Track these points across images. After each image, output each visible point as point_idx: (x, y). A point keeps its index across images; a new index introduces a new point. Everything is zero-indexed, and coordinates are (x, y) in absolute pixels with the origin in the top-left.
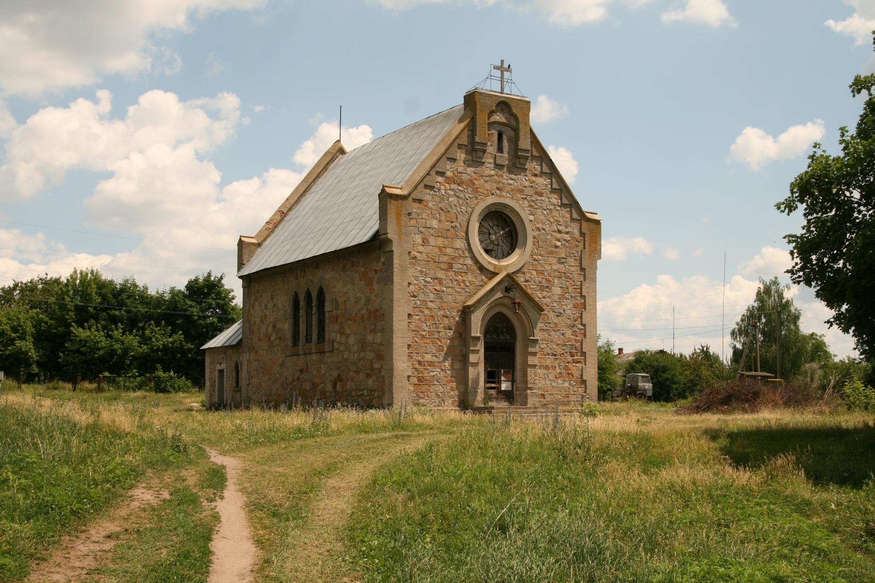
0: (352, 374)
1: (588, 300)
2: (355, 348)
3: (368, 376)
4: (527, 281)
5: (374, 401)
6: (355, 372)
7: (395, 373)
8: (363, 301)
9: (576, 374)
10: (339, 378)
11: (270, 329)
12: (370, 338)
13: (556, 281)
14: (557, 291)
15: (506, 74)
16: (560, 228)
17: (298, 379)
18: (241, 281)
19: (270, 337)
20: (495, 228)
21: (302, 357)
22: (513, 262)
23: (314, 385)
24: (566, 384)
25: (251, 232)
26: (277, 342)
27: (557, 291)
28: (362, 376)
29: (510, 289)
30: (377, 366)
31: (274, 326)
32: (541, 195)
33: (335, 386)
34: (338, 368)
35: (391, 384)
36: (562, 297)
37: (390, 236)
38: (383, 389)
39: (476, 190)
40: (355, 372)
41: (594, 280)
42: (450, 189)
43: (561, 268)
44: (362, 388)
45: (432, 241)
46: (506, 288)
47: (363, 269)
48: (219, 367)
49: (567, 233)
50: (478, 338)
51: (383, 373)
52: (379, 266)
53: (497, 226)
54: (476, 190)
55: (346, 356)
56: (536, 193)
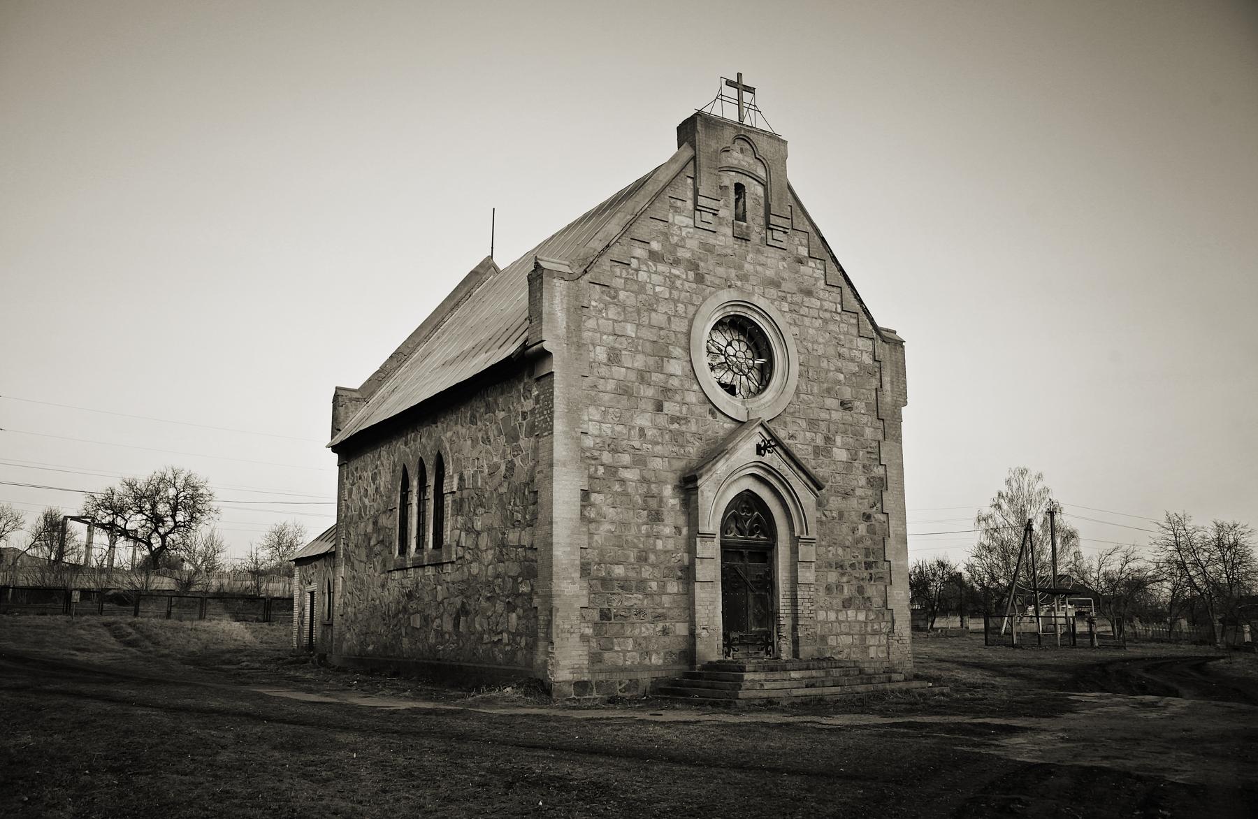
0: (484, 604)
1: (892, 473)
2: (489, 556)
3: (511, 607)
4: (792, 437)
5: (519, 654)
6: (488, 599)
7: (556, 602)
8: (503, 467)
9: (877, 602)
10: (463, 611)
11: (370, 528)
12: (512, 537)
13: (838, 439)
14: (841, 455)
15: (747, 96)
16: (842, 350)
17: (405, 609)
18: (336, 456)
19: (370, 540)
20: (735, 344)
21: (411, 572)
22: (767, 405)
23: (426, 620)
24: (862, 617)
25: (355, 382)
26: (378, 548)
27: (841, 455)
28: (500, 607)
29: (765, 448)
30: (524, 589)
31: (375, 523)
32: (809, 293)
33: (456, 625)
34: (462, 592)
35: (549, 623)
36: (849, 465)
37: (547, 346)
38: (534, 635)
39: (700, 279)
40: (488, 599)
41: (898, 439)
42: (655, 272)
43: (847, 416)
44: (500, 628)
45: (626, 360)
46: (758, 446)
47: (501, 415)
48: (310, 588)
49: (852, 360)
50: (712, 536)
51: (536, 601)
52: (528, 405)
53: (739, 341)
54: (700, 279)
55: (475, 570)
56: (801, 291)
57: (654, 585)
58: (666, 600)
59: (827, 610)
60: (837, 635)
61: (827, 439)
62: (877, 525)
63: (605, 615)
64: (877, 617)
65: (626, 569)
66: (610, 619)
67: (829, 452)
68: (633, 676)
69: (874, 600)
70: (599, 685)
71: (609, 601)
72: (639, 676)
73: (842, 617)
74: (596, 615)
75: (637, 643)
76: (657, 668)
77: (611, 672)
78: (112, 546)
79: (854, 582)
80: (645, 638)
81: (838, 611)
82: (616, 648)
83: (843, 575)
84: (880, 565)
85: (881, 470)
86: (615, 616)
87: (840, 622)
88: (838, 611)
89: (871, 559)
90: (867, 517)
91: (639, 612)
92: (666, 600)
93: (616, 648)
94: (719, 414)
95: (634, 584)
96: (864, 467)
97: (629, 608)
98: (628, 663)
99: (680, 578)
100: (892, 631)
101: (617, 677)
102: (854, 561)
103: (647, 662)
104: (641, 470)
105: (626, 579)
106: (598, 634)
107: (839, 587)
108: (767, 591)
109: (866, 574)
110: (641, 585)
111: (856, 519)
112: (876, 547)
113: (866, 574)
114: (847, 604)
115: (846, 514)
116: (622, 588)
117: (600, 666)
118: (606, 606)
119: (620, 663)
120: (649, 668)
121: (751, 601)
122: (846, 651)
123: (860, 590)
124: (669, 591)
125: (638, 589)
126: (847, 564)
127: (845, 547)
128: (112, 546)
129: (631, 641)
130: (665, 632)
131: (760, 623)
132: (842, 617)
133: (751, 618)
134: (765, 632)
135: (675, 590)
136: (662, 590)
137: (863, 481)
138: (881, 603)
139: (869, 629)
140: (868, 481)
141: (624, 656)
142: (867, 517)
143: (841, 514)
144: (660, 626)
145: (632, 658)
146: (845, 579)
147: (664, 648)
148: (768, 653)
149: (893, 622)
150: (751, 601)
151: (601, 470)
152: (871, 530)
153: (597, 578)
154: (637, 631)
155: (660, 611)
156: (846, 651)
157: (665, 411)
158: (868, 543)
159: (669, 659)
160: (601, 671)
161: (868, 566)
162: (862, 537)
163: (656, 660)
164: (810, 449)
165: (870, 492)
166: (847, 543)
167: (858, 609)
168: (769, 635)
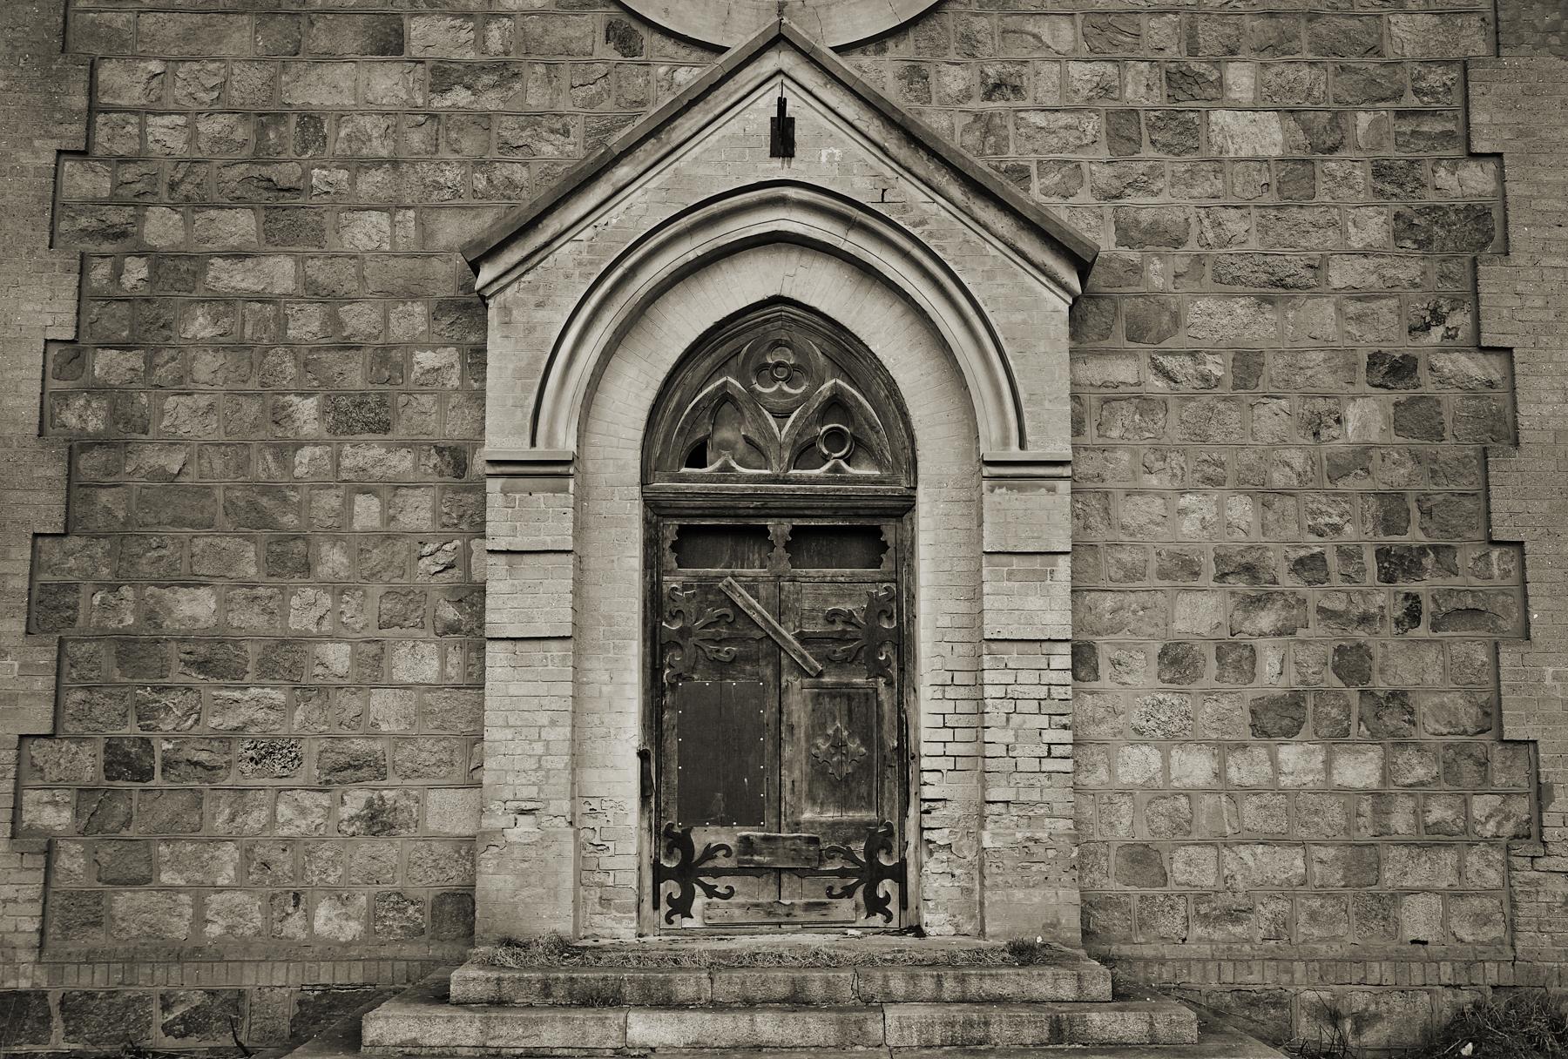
13: (1241, 79)
14: (1250, 132)
36: (1295, 175)
57: (337, 657)
58: (386, 708)
59: (1171, 740)
60: (1220, 843)
61: (1179, 80)
62: (1452, 400)
63: (126, 763)
64: (1449, 771)
65: (225, 603)
66: (147, 775)
67: (1188, 129)
68: (222, 979)
69: (1424, 705)
70: (74, 1007)
71: (145, 713)
72: (249, 979)
73: (1241, 771)
74: (88, 764)
75: (254, 864)
76: (334, 952)
77: (131, 960)
78: (1166, 759)
79: (1316, 629)
80: (289, 842)
81: (1224, 749)
82: (166, 878)
83: (1257, 602)
84: (1466, 557)
85: (1477, 180)
86: (168, 765)
87: (1236, 793)
88: (1224, 749)
89: (1415, 536)
90: (1394, 370)
91: (265, 753)
92: (386, 708)
93: (166, 878)
94: (651, 40)
95: (252, 651)
96: (1380, 171)
97: (226, 739)
98: (214, 930)
99: (452, 628)
100: (1531, 834)
101: (151, 980)
102: (1314, 544)
103: (294, 927)
104: (300, 261)
105: (220, 638)
106: (91, 825)
107: (1236, 655)
108: (879, 670)
109: (1384, 599)
110: (285, 658)
111: (1327, 381)
112: (1437, 490)
113: (1384, 599)
114: (1278, 719)
115: (1275, 366)
116: (203, 666)
117: (97, 939)
118: (132, 729)
119: (180, 928)
120: (291, 953)
121: (798, 707)
122: (1267, 910)
123: (1352, 664)
124: (401, 674)
125: (267, 670)
126: (1277, 560)
127: (1265, 495)
128: (1166, 759)
129: (229, 854)
130: (377, 821)
131: (833, 782)
132: (1241, 771)
133: (794, 773)
134: (862, 829)
135: (429, 670)
136: (373, 667)
137: (1373, 227)
138: (1468, 717)
139: (1401, 821)
140: (1403, 227)
141: (200, 906)
142: (1394, 370)
143: (1247, 364)
144: (355, 801)
145: (233, 913)
146: (1266, 620)
147: (371, 878)
148: (875, 905)
149: (1541, 794)
150: (798, 707)
151: (136, 272)
152: (1418, 420)
153: (101, 636)
154: (255, 820)
155: (359, 746)
156: (1267, 910)
157: (414, 49)
158: (1398, 474)
159: (394, 922)
160: (91, 958)
161: (1396, 564)
162: (1366, 450)
163: (328, 921)
164: (1092, 125)
165: (1410, 270)
166: (1279, 478)
167: (1338, 737)
168: (882, 838)
